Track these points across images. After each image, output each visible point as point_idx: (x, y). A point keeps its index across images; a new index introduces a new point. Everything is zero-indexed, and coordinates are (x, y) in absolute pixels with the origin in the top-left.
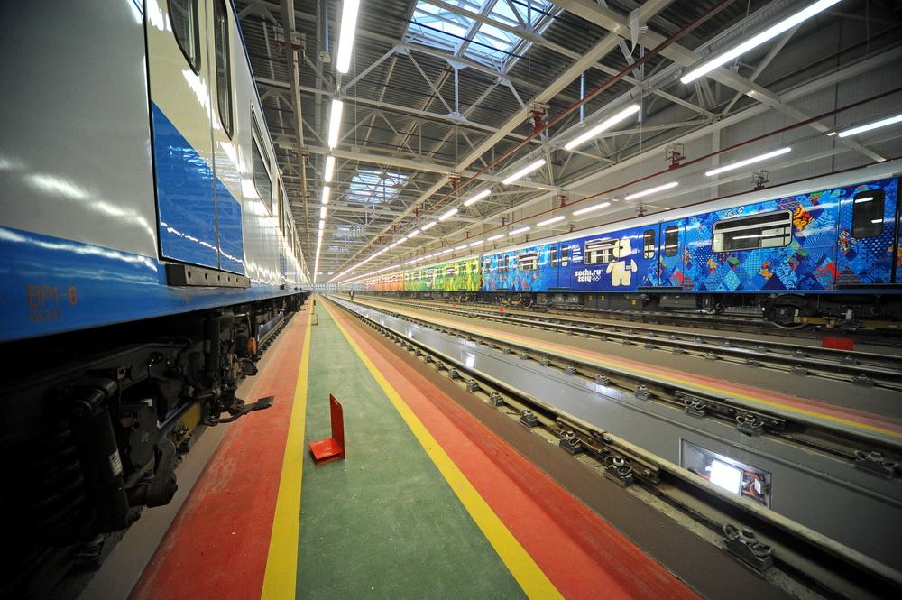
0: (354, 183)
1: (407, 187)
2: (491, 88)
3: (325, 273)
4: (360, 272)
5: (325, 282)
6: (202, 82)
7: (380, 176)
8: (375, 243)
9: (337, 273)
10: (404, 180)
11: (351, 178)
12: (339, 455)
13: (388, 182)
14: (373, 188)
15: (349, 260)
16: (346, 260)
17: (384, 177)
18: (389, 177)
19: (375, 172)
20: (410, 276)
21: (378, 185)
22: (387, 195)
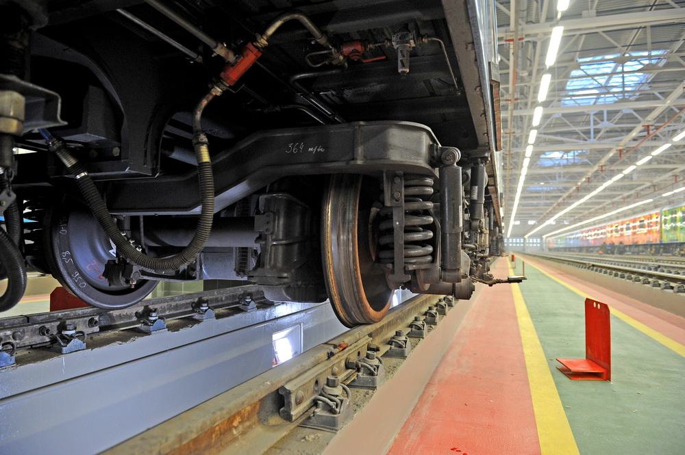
0: (573, 78)
1: (666, 66)
2: (267, 191)
3: (524, 222)
4: (576, 217)
5: (522, 236)
6: (102, 196)
7: (614, 60)
8: (612, 161)
9: (541, 222)
10: (659, 58)
11: (569, 73)
12: (603, 374)
13: (630, 66)
14: (602, 81)
15: (565, 195)
16: (557, 200)
17: (621, 61)
18: (631, 59)
19: (607, 57)
20: (674, 220)
21: (611, 75)
22: (626, 89)
